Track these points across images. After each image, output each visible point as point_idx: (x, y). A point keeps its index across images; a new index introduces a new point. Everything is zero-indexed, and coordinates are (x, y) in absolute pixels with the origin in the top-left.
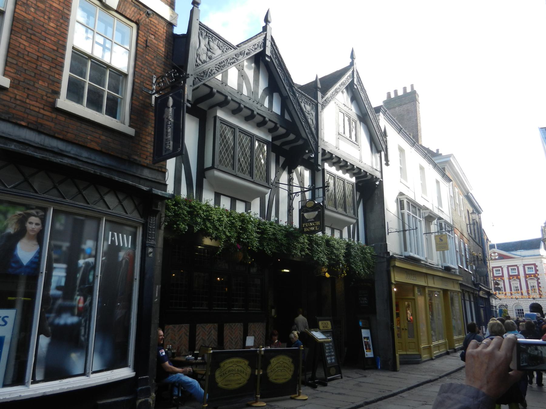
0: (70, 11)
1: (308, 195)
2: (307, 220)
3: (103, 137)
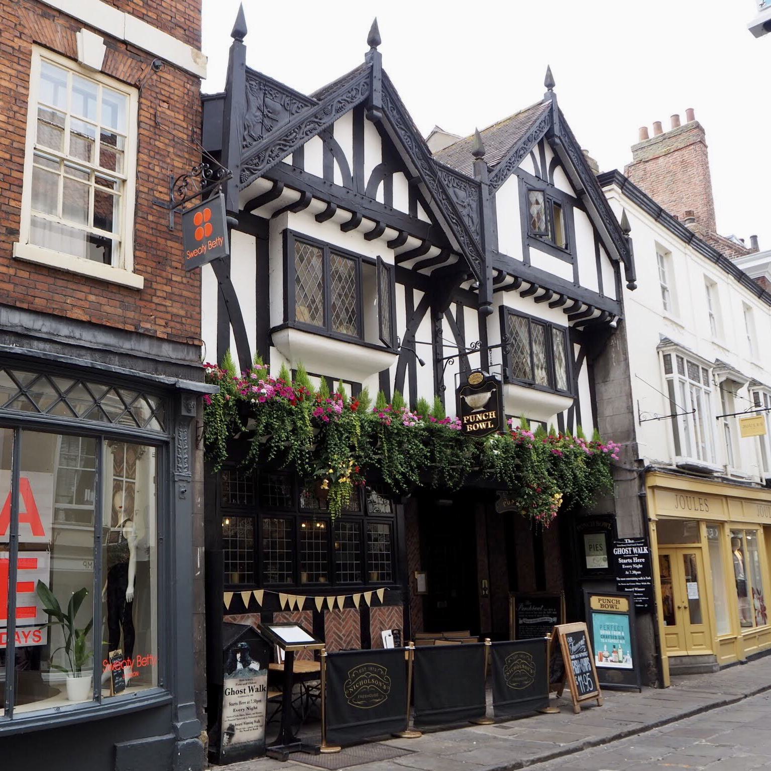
0: (27, 89)
1: (475, 361)
3: (92, 298)
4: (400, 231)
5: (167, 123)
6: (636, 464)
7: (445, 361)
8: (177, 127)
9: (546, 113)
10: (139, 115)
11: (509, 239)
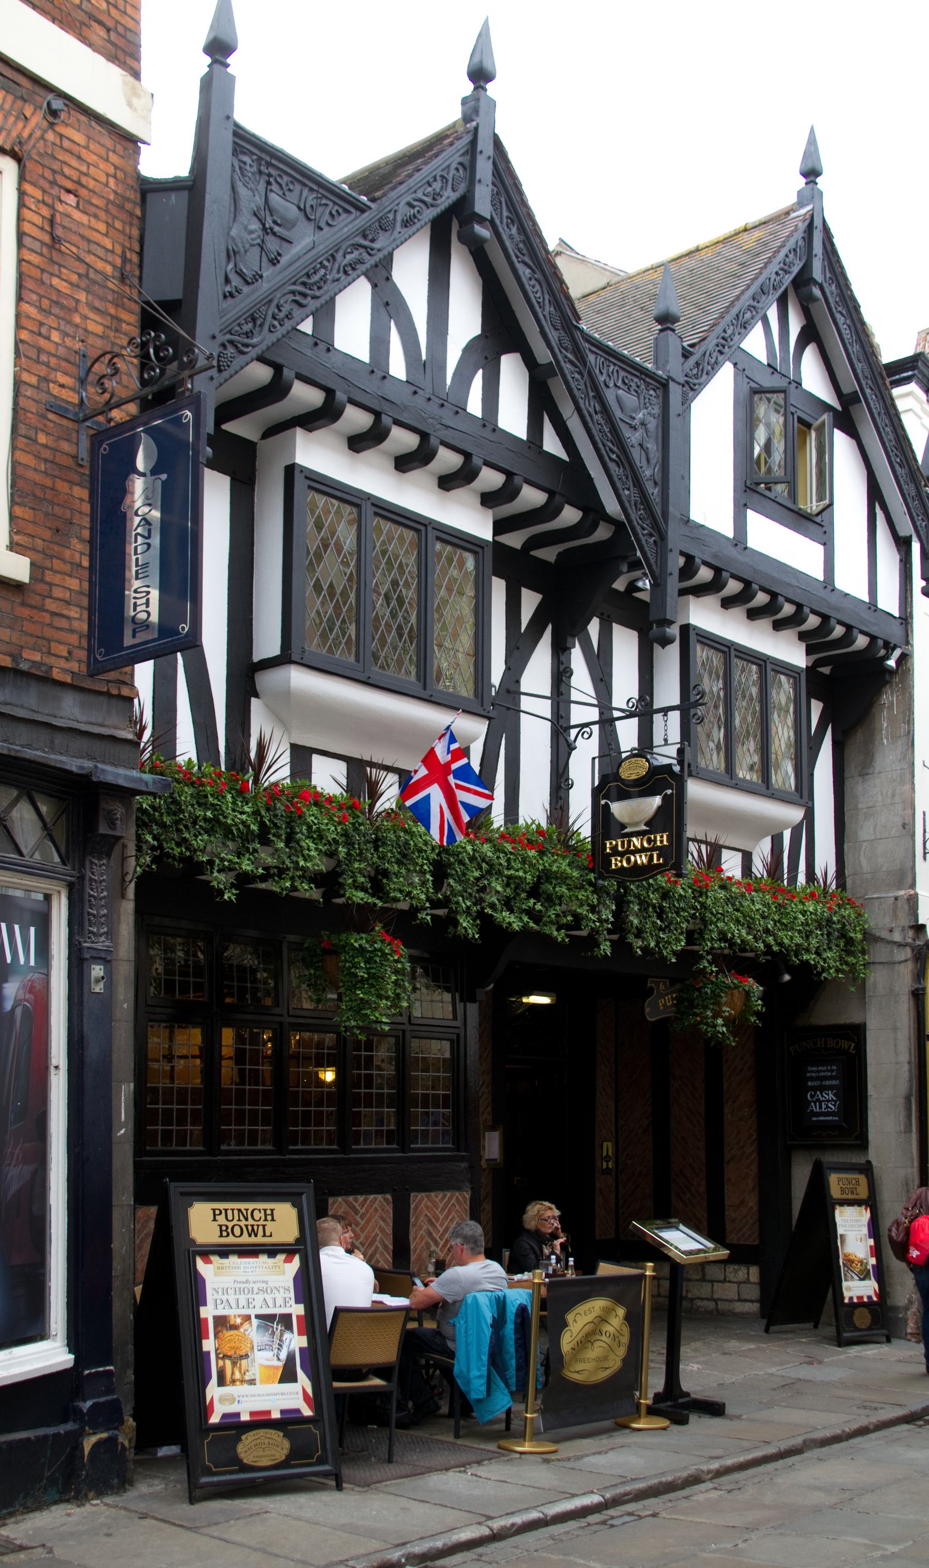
1: (628, 734)
2: (623, 826)
4: (509, 475)
5: (75, 239)
7: (573, 732)
8: (93, 247)
9: (799, 235)
10: (20, 219)
11: (710, 496)
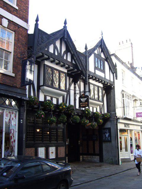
6: (116, 117)
